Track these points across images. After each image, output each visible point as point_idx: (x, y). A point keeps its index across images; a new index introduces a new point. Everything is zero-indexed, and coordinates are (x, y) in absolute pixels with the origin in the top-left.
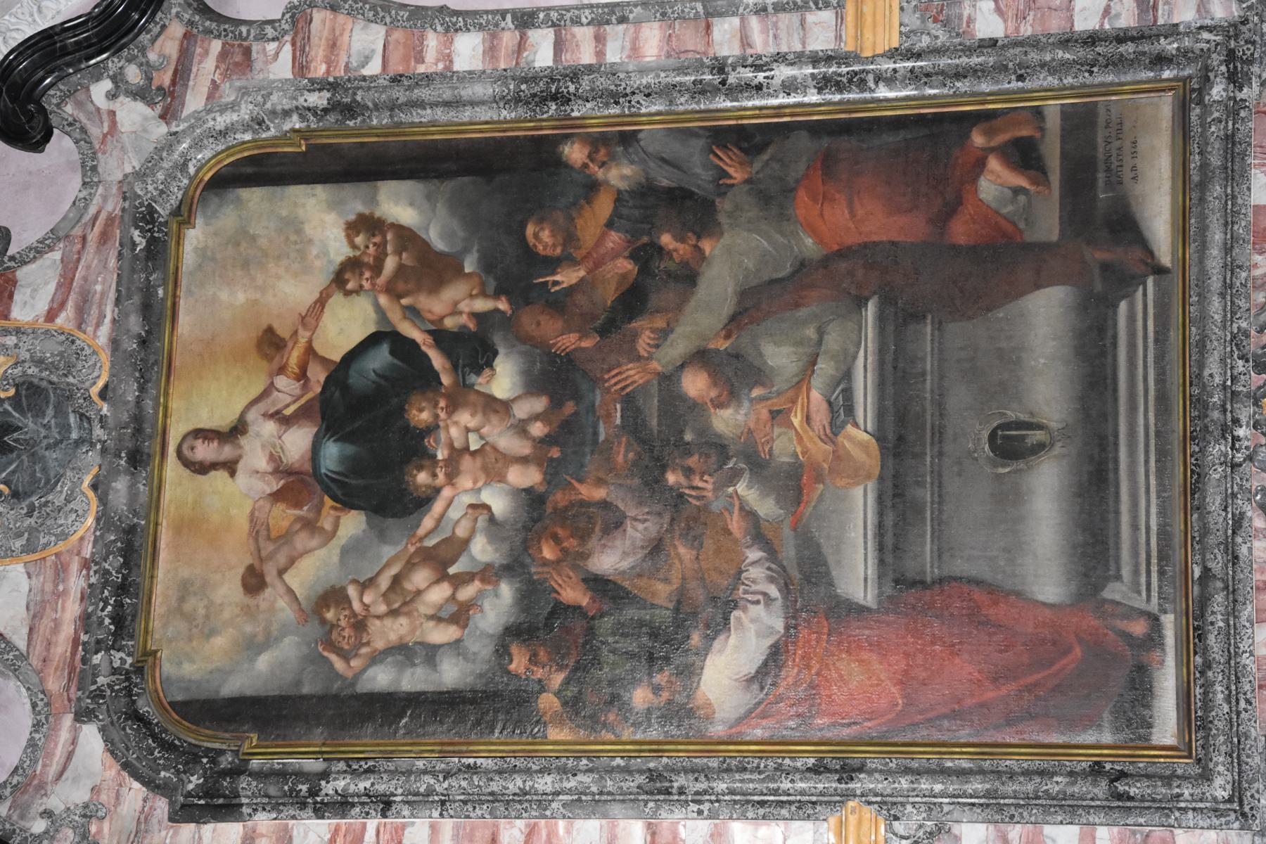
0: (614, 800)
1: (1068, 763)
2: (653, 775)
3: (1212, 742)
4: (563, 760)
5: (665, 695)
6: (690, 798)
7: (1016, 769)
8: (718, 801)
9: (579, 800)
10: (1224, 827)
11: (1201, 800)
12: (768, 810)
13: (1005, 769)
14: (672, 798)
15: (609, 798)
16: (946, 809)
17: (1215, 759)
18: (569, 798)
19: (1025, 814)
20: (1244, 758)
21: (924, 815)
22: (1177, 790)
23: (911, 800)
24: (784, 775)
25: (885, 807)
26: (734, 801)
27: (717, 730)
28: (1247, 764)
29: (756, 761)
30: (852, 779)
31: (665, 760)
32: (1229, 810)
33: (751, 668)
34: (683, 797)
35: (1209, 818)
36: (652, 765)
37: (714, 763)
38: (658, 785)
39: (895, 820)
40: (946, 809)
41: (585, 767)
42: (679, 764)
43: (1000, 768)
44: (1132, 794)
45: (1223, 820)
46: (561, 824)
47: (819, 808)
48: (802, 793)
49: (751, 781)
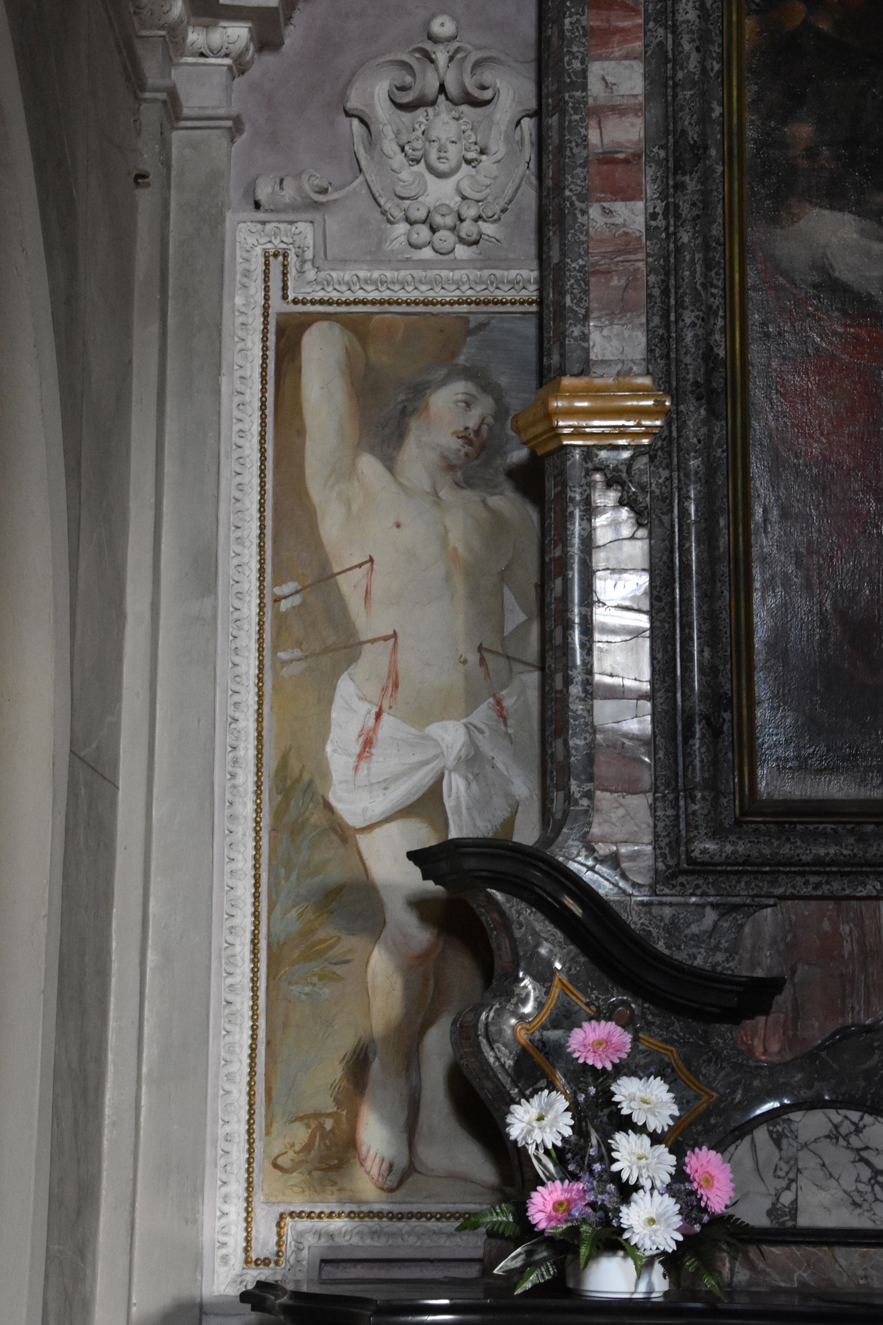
0: (667, 106)
1: (728, 666)
2: (699, 151)
3: (762, 840)
4: (718, 40)
5: (804, 163)
6: (671, 200)
7: (719, 604)
8: (668, 236)
9: (667, 61)
10: (658, 852)
11: (688, 825)
12: (658, 300)
13: (718, 590)
14: (671, 176)
15: (670, 98)
16: (665, 519)
17: (740, 843)
18: (670, 48)
19: (663, 615)
20: (745, 879)
21: (657, 492)
22: (699, 795)
23: (675, 474)
24: (701, 314)
25: (665, 444)
26: (669, 257)
27: (755, 234)
28: (739, 881)
29: (720, 283)
30: (698, 399)
31: (719, 169)
32: (679, 858)
33: (843, 272)
34: (671, 191)
35: (668, 835)
36: (713, 152)
37: (716, 231)
38: (687, 156)
39: (650, 457)
40: (665, 519)
41: (709, 67)
42: (714, 187)
43: (719, 585)
44: (691, 742)
45: (667, 851)
46: (638, 45)
47: (662, 362)
48: (680, 339)
49: (693, 274)
